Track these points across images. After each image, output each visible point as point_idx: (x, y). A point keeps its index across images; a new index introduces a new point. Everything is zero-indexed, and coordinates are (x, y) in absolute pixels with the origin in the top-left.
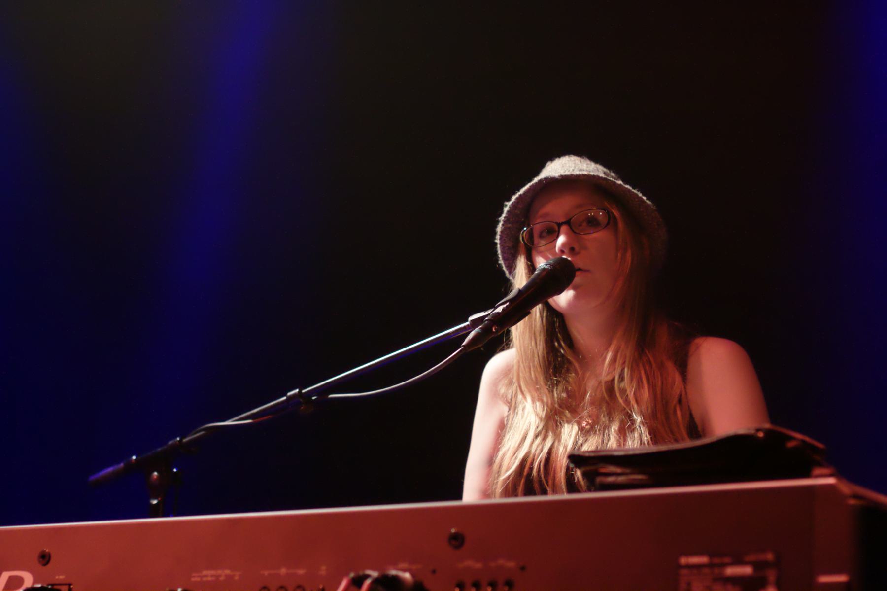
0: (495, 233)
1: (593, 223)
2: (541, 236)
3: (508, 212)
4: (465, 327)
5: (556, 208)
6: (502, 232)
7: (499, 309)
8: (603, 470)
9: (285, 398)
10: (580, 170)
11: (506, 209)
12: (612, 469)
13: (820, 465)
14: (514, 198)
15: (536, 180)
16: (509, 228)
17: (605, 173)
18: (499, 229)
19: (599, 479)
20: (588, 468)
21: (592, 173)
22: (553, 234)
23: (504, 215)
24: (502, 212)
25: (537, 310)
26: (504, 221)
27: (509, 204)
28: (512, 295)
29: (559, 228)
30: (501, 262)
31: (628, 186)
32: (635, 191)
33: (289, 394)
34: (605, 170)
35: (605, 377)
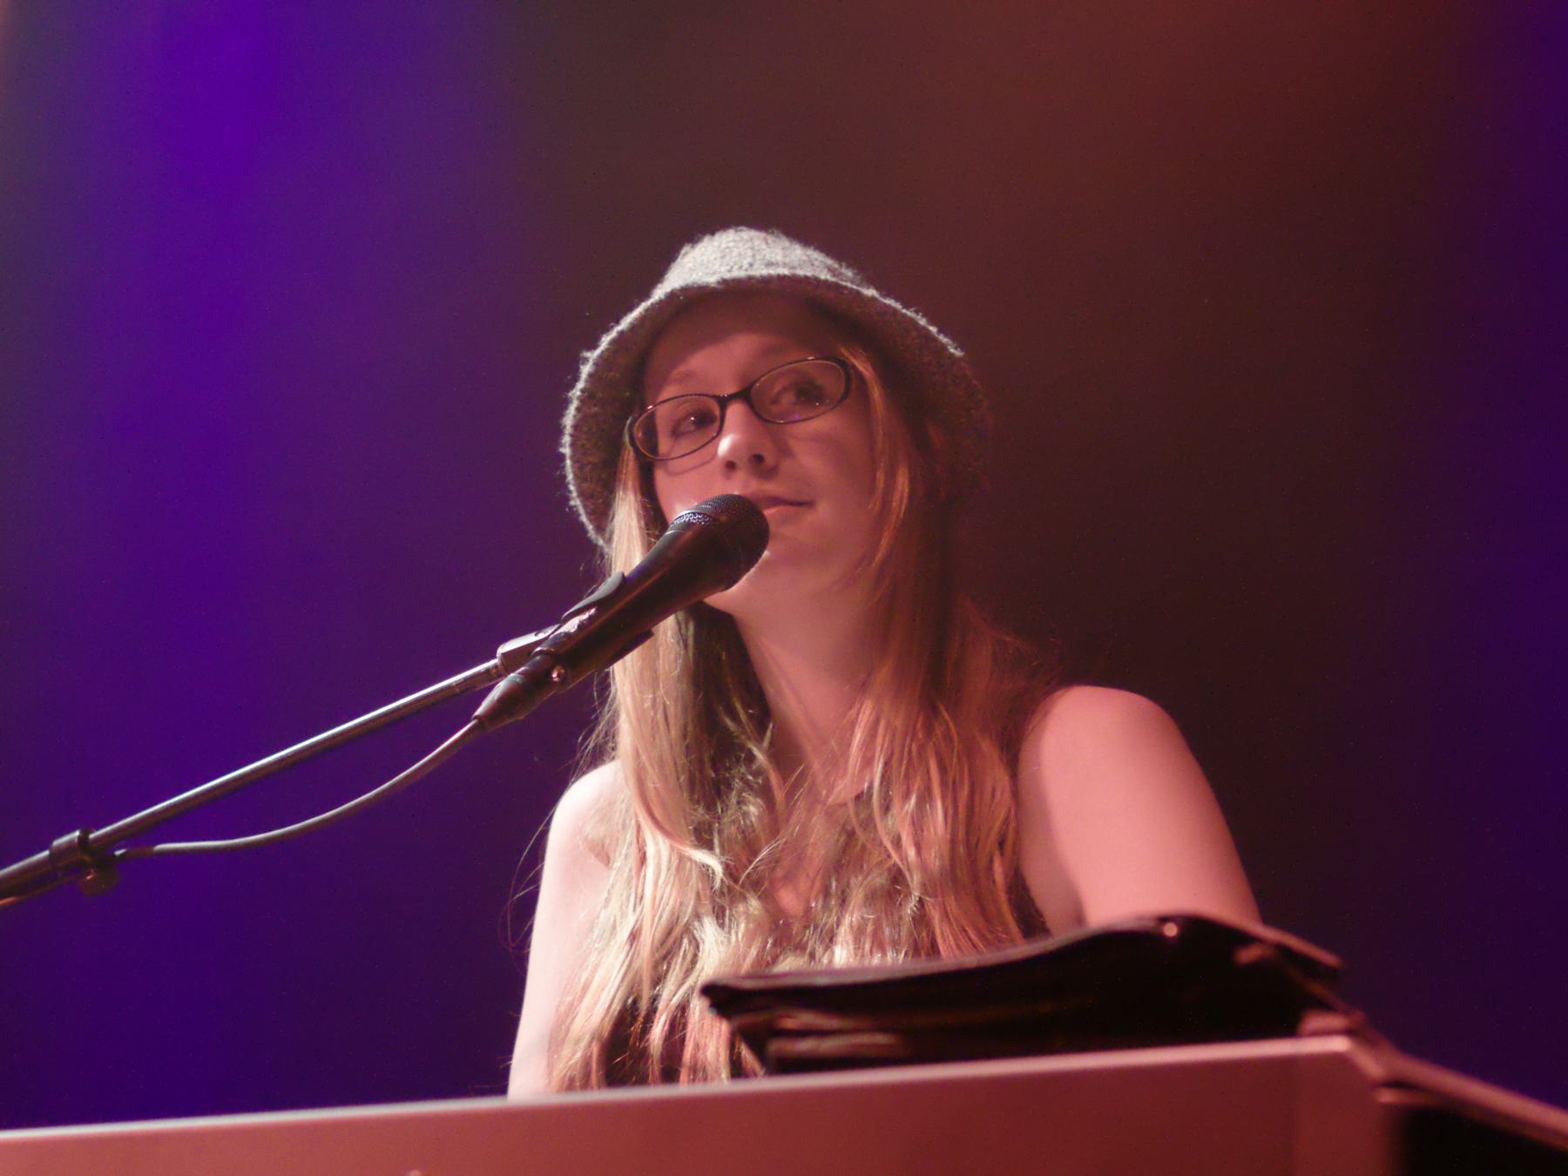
0: (559, 432)
1: (809, 395)
2: (676, 433)
3: (590, 375)
4: (487, 671)
5: (717, 364)
6: (576, 427)
7: (571, 626)
8: (789, 1023)
9: (46, 853)
10: (770, 264)
11: (586, 370)
12: (805, 1019)
13: (1325, 1007)
14: (605, 341)
15: (659, 293)
16: (595, 416)
17: (830, 269)
18: (569, 420)
19: (775, 1047)
20: (749, 1019)
21: (800, 273)
22: (707, 421)
23: (580, 385)
24: (576, 379)
25: (668, 628)
26: (582, 400)
27: (593, 355)
28: (604, 589)
29: (723, 409)
30: (576, 502)
31: (890, 302)
32: (910, 313)
33: (56, 843)
34: (829, 262)
35: (843, 789)
